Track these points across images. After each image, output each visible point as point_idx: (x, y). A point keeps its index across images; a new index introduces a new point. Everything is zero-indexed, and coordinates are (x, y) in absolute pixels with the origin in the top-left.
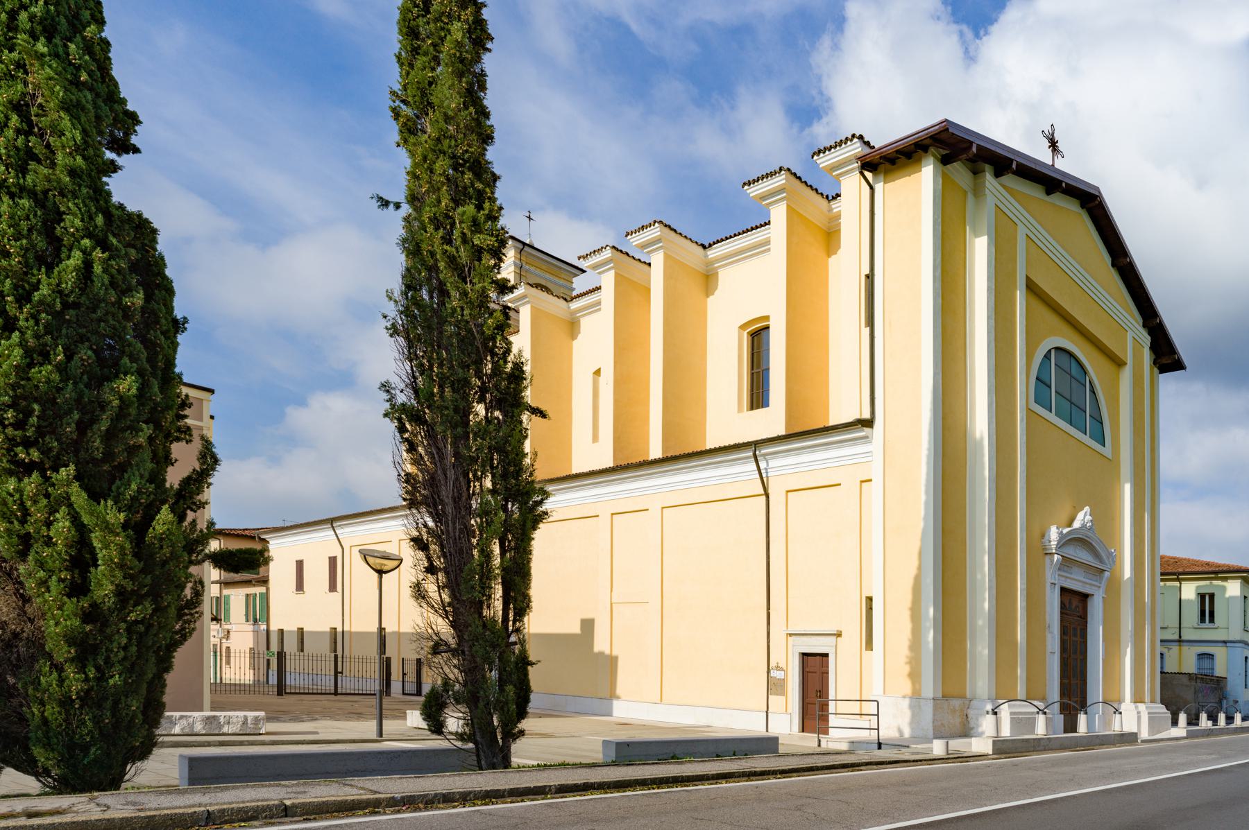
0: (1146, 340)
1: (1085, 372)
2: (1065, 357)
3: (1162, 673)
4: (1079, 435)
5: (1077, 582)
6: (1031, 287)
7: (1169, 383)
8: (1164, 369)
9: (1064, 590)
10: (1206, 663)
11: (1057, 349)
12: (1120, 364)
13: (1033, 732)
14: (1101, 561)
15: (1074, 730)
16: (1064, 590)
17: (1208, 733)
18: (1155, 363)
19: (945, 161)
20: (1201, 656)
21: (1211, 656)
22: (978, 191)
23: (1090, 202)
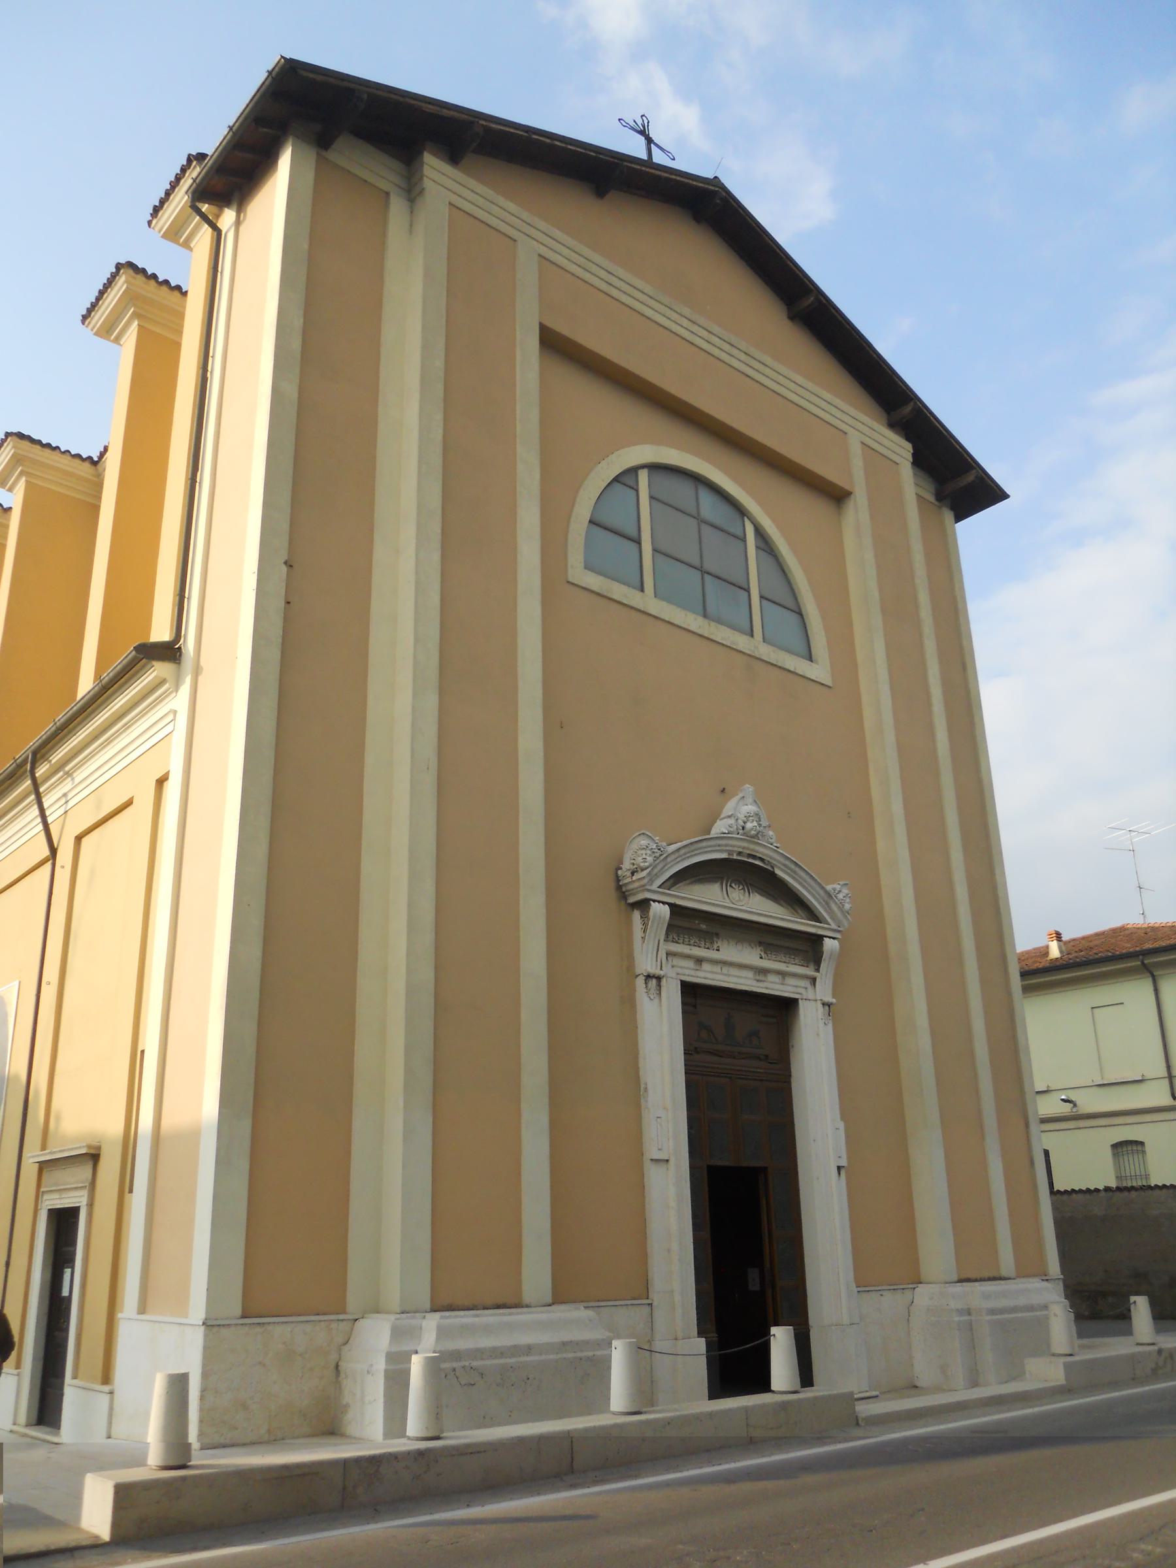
0: (901, 450)
1: (740, 511)
2: (682, 491)
3: (1052, 1192)
4: (742, 642)
5: (736, 967)
6: (554, 344)
7: (974, 534)
8: (963, 511)
9: (691, 991)
10: (1131, 1165)
11: (655, 468)
12: (837, 496)
13: (330, 1426)
14: (813, 916)
15: (760, 1381)
16: (691, 991)
17: (784, 1429)
18: (940, 497)
19: (323, 141)
20: (1119, 1147)
21: (1137, 1145)
22: (412, 191)
23: (710, 209)
